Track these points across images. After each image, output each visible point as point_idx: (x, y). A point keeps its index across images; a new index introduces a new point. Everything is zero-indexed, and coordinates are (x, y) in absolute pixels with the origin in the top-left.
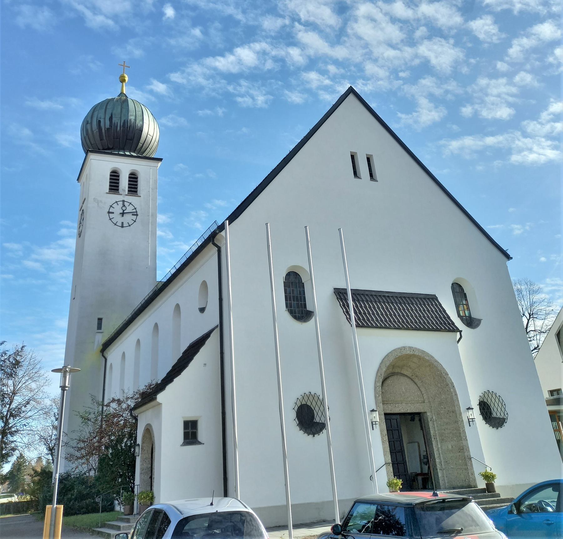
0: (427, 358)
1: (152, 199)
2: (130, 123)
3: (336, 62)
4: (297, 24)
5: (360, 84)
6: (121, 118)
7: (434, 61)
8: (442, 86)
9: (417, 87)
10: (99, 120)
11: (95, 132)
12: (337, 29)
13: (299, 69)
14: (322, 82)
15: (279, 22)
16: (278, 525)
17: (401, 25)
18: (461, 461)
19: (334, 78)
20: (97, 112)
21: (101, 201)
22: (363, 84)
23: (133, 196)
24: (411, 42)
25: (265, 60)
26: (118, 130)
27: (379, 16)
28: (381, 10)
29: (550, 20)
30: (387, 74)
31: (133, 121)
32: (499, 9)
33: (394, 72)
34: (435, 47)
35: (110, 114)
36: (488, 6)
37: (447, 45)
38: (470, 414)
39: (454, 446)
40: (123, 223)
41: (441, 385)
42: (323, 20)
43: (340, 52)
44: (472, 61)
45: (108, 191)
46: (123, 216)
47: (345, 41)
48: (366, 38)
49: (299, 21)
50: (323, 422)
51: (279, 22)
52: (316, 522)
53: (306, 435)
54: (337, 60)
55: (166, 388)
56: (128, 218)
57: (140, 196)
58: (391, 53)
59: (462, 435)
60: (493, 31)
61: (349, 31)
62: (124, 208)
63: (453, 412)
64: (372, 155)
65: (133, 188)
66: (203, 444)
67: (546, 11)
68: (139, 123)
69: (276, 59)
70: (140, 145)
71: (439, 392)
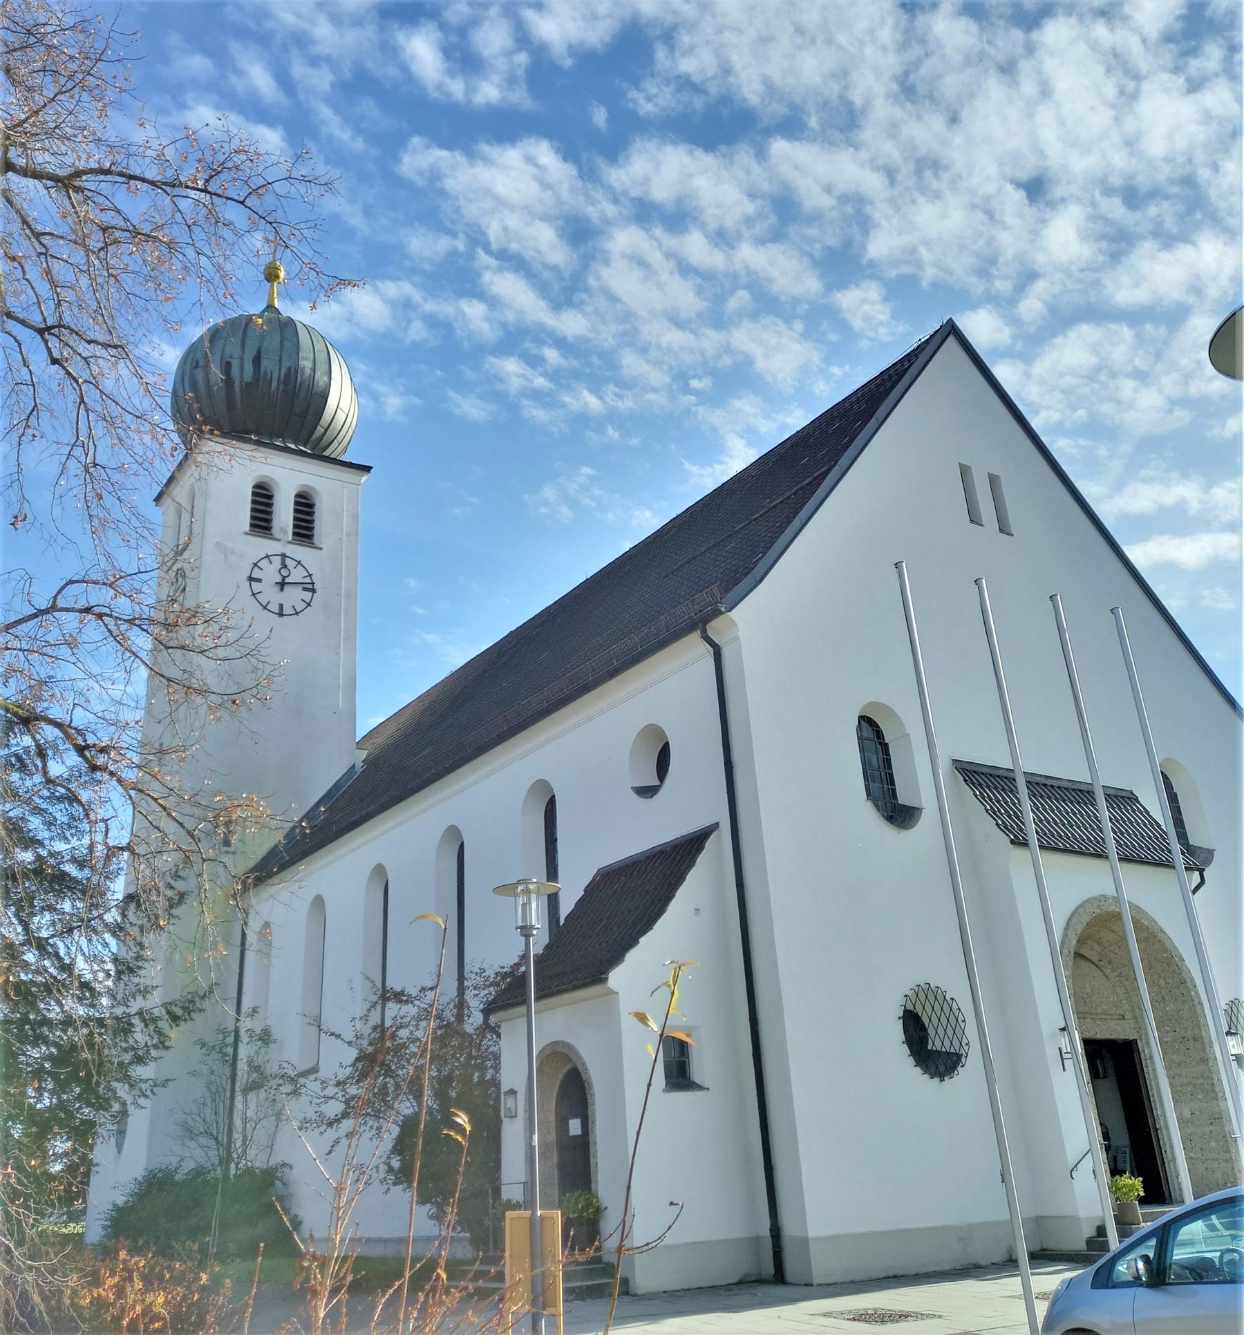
0: (1146, 923)
1: (347, 559)
2: (302, 377)
3: (561, 343)
4: (480, 252)
5: (610, 393)
6: (280, 361)
7: (761, 365)
8: (774, 415)
9: (724, 414)
10: (230, 360)
11: (216, 387)
12: (567, 275)
13: (480, 350)
14: (531, 381)
15: (444, 244)
16: (892, 1275)
17: (699, 281)
18: (1214, 1144)
19: (554, 376)
20: (222, 341)
21: (232, 551)
22: (616, 395)
23: (304, 545)
24: (719, 320)
25: (409, 321)
26: (273, 389)
27: (655, 258)
28: (660, 245)
29: (989, 307)
30: (667, 380)
31: (308, 371)
32: (893, 273)
33: (681, 378)
34: (765, 336)
35: (256, 349)
36: (871, 264)
37: (790, 333)
38: (510, 1102)
39: (1197, 1113)
40: (281, 606)
41: (1167, 983)
42: (539, 252)
43: (572, 324)
44: (836, 371)
45: (247, 528)
46: (282, 590)
47: (582, 302)
48: (625, 299)
49: (486, 247)
50: (939, 1050)
51: (444, 244)
52: (961, 1268)
53: (927, 1076)
54: (565, 338)
55: (625, 959)
56: (294, 596)
57: (321, 549)
58: (674, 337)
59: (1217, 1088)
60: (882, 317)
61: (592, 282)
62: (285, 573)
63: (1195, 1039)
64: (998, 476)
65: (304, 529)
66: (705, 1089)
67: (982, 288)
68: (321, 379)
69: (432, 322)
70: (320, 430)
71: (1160, 997)
